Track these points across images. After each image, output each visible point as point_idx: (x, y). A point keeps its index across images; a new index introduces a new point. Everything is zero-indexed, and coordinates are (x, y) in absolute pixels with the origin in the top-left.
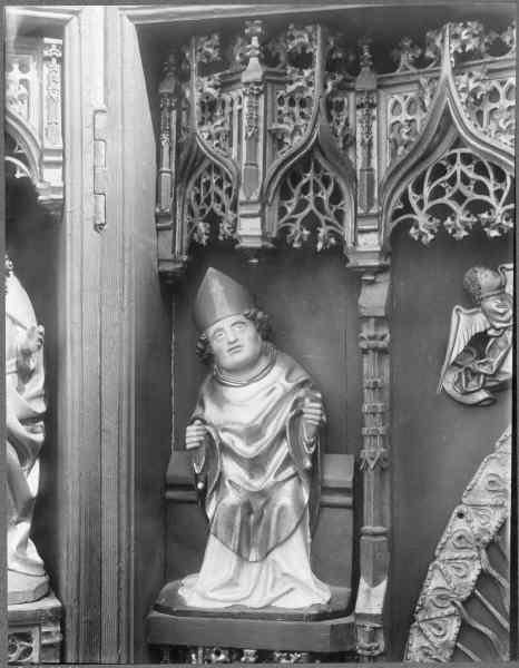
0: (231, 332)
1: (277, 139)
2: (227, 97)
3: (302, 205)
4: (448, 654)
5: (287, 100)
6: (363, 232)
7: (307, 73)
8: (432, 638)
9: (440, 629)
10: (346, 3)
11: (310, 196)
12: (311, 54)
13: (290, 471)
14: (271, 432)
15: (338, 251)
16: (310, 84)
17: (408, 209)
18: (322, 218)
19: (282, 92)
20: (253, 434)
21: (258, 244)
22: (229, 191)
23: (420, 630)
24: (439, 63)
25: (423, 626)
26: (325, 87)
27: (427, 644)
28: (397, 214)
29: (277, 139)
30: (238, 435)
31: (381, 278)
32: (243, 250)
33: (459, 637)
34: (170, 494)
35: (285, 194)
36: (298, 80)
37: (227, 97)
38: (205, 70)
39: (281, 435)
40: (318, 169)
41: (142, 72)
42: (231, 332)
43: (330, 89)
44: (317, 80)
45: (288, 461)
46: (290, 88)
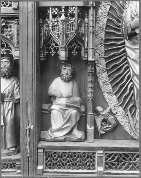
1: (67, 36)
4: (107, 14)
5: (69, 25)
7: (74, 19)
8: (104, 10)
9: (105, 8)
12: (74, 14)
16: (75, 10)
19: (68, 23)
21: (64, 59)
23: (101, 8)
25: (101, 7)
26: (78, 21)
27: (103, 11)
29: (67, 36)
32: (60, 60)
33: (110, 10)
34: (43, 112)
36: (72, 21)
40: (76, 43)
41: (52, 124)
43: (79, 22)
44: (76, 20)
46: (70, 22)
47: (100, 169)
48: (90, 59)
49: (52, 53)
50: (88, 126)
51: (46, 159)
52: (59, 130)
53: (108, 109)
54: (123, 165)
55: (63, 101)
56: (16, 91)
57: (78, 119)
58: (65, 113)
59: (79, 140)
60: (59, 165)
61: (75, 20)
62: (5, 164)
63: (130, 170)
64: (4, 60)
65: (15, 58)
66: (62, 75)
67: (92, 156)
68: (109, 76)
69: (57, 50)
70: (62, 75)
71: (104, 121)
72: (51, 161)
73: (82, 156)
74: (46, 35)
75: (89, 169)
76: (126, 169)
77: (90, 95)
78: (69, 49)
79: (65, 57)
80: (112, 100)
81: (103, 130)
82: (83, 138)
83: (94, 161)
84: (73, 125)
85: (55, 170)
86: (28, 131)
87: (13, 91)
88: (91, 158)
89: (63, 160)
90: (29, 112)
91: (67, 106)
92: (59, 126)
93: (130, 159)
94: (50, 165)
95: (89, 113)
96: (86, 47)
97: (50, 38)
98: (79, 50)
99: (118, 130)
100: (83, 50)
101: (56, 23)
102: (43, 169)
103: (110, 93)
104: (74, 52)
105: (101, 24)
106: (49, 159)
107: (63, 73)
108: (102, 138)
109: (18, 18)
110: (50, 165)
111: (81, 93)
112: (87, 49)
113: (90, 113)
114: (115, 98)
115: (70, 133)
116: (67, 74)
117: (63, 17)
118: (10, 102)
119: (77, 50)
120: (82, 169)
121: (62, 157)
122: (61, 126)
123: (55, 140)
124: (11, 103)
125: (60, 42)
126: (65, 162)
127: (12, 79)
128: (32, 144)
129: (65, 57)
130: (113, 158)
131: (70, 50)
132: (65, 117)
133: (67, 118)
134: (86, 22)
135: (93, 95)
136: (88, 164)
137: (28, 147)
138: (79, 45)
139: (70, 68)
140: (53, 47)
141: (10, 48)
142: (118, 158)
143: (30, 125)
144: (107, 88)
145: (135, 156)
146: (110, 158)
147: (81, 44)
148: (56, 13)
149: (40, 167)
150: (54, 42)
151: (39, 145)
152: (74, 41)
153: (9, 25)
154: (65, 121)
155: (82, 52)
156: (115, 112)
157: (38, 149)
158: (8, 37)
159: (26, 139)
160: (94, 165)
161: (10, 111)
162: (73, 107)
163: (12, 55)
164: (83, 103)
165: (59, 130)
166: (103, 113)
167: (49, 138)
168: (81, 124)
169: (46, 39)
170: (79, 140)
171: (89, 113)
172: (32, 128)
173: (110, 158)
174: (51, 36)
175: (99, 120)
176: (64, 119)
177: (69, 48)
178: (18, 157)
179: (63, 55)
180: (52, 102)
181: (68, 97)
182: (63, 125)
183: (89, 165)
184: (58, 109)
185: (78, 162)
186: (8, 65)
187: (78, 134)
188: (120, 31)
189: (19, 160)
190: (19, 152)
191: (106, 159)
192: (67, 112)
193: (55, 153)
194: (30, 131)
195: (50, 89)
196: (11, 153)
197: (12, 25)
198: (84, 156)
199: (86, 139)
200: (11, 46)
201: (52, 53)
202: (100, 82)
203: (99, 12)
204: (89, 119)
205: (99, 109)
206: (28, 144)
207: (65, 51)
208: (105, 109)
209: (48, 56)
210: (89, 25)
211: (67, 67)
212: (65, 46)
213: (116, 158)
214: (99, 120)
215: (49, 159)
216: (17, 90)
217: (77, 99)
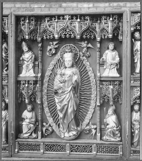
0: (25, 48)
1: (29, 93)
3: (32, 35)
13: (31, 62)
14: (29, 58)
15: (36, 40)
17: (43, 36)
20: (27, 59)
38: (22, 21)
39: (31, 59)
45: (31, 61)
47: (95, 153)
51: (20, 147)
52: (26, 133)
53: (49, 124)
54: (53, 149)
55: (28, 121)
56: (7, 116)
59: (35, 138)
61: (32, 86)
63: (55, 152)
65: (7, 103)
67: (39, 145)
68: (49, 109)
69: (25, 98)
71: (46, 129)
73: (36, 145)
76: (54, 151)
80: (50, 120)
85: (24, 151)
86: (11, 134)
87: (6, 116)
88: (39, 146)
93: (56, 147)
94: (21, 149)
98: (35, 98)
99: (54, 133)
102: (43, 152)
103: (50, 117)
104: (33, 100)
106: (21, 146)
108: (45, 137)
110: (21, 149)
114: (52, 119)
115: (31, 135)
117: (27, 85)
119: (34, 98)
123: (24, 138)
126: (27, 148)
127: (6, 111)
128: (13, 140)
130: (48, 146)
131: (31, 99)
137: (11, 141)
138: (35, 96)
139: (31, 106)
142: (50, 147)
144: (48, 115)
145: (82, 146)
146: (47, 147)
148: (24, 83)
149: (16, 150)
152: (32, 94)
153: (4, 88)
155: (36, 99)
156: (52, 126)
161: (4, 125)
162: (32, 123)
163: (5, 101)
164: (37, 121)
165: (26, 133)
166: (46, 126)
167: (22, 137)
168: (35, 131)
170: (35, 138)
173: (47, 147)
175: (44, 129)
176: (28, 128)
177: (30, 98)
178: (7, 145)
180: (23, 121)
181: (30, 119)
182: (28, 131)
188: (53, 89)
189: (8, 147)
190: (8, 143)
191: (45, 147)
193: (23, 144)
197: (6, 88)
200: (5, 97)
202: (45, 112)
205: (44, 124)
207: (28, 99)
208: (47, 124)
209: (22, 100)
212: (28, 97)
213: (50, 146)
214: (44, 129)
216: (8, 116)
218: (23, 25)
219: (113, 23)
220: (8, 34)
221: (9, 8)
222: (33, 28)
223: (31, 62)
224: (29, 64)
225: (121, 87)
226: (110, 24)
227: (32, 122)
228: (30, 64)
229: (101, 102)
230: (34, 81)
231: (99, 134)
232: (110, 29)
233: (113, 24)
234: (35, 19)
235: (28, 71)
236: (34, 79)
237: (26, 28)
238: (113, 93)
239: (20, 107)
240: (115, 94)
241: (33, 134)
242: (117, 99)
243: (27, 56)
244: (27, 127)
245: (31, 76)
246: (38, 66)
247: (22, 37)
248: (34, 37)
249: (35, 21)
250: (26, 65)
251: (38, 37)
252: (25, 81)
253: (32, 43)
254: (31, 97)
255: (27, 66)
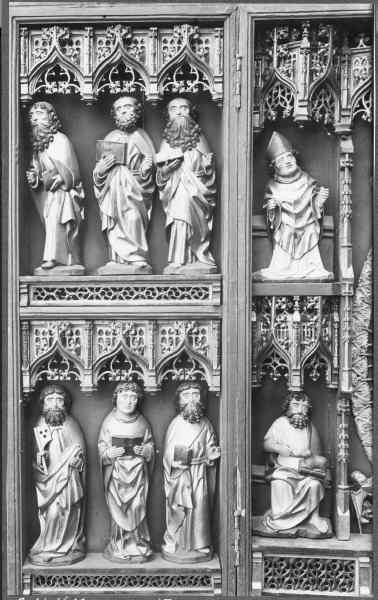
0: (284, 159)
2: (292, 54)
3: (320, 103)
6: (344, 116)
7: (315, 318)
10: (81, 596)
11: (323, 100)
13: (311, 221)
14: (304, 203)
15: (330, 127)
17: (362, 107)
18: (327, 110)
20: (297, 202)
22: (289, 97)
24: (33, 570)
28: (357, 109)
30: (291, 204)
31: (350, 137)
35: (314, 99)
37: (292, 54)
38: (280, 42)
39: (309, 205)
42: (284, 159)
45: (311, 215)
48: (345, 388)
49: (274, 376)
50: (338, 508)
51: (266, 571)
52: (286, 517)
55: (294, 464)
57: (322, 497)
58: (297, 486)
59: (323, 537)
60: (289, 582)
62: (74, 577)
64: (192, 390)
66: (293, 415)
67: (348, 568)
70: (293, 415)
72: (275, 574)
74: (264, 344)
75: (344, 590)
77: (342, 453)
78: (307, 372)
79: (301, 387)
81: (365, 517)
82: (330, 531)
83: (352, 575)
84: (312, 509)
89: (296, 572)
90: (239, 486)
91: (301, 473)
92: (286, 506)
94: (273, 581)
95: (340, 486)
96: (336, 366)
97: (271, 349)
98: (322, 370)
100: (329, 369)
101: (283, 325)
105: (361, 319)
106: (271, 570)
107: (294, 412)
109: (221, 320)
111: (324, 446)
112: (338, 369)
113: (343, 485)
116: (300, 414)
118: (200, 464)
119: (318, 370)
120: (331, 591)
121: (294, 567)
122: (291, 508)
123: (279, 535)
124: (202, 467)
125: (293, 359)
129: (301, 387)
132: (297, 492)
133: (302, 496)
134: (336, 319)
135: (349, 452)
136: (342, 580)
138: (322, 361)
139: (306, 403)
140: (275, 365)
141: (203, 370)
143: (239, 508)
147: (326, 359)
150: (278, 356)
151: (255, 546)
154: (299, 500)
155: (328, 372)
157: (252, 552)
158: (202, 352)
159: (232, 537)
160: (351, 583)
165: (286, 517)
167: (269, 531)
168: (327, 508)
169: (263, 351)
170: (323, 537)
171: (340, 486)
172: (243, 514)
174: (273, 346)
176: (296, 495)
178: (214, 565)
179: (295, 383)
183: (343, 584)
184: (285, 477)
185: (323, 576)
186: (197, 399)
187: (320, 525)
192: (301, 484)
193: (282, 559)
194: (239, 521)
195: (269, 438)
196: (203, 557)
197: (80, 329)
198: (335, 566)
199: (333, 533)
200: (204, 366)
201: (274, 376)
203: (358, 298)
204: (340, 496)
206: (236, 543)
210: (343, 329)
211: (301, 402)
214: (358, 499)
215: (271, 570)
217: (320, 460)
218: (282, 59)
219: (312, 58)
220: (221, 101)
221: (18, 10)
222: (325, 71)
223: (311, 221)
224: (302, 229)
225: (333, 322)
226: (300, 60)
227: (315, 471)
228: (307, 225)
229: (26, 383)
230: (323, 297)
231: (345, 512)
232: (300, 85)
233: (311, 63)
234: (333, 38)
235: (297, 256)
236: (328, 290)
237: (298, 70)
238: (302, 347)
239: (266, 402)
240: (309, 350)
241: (316, 520)
242: (318, 370)
243: (291, 192)
244: (293, 489)
245: (313, 276)
246: (331, 235)
247: (273, 113)
248: (323, 111)
249: (335, 44)
250: (293, 231)
251: (341, 109)
252: (290, 298)
253: (311, 138)
254: (308, 366)
255: (295, 236)
